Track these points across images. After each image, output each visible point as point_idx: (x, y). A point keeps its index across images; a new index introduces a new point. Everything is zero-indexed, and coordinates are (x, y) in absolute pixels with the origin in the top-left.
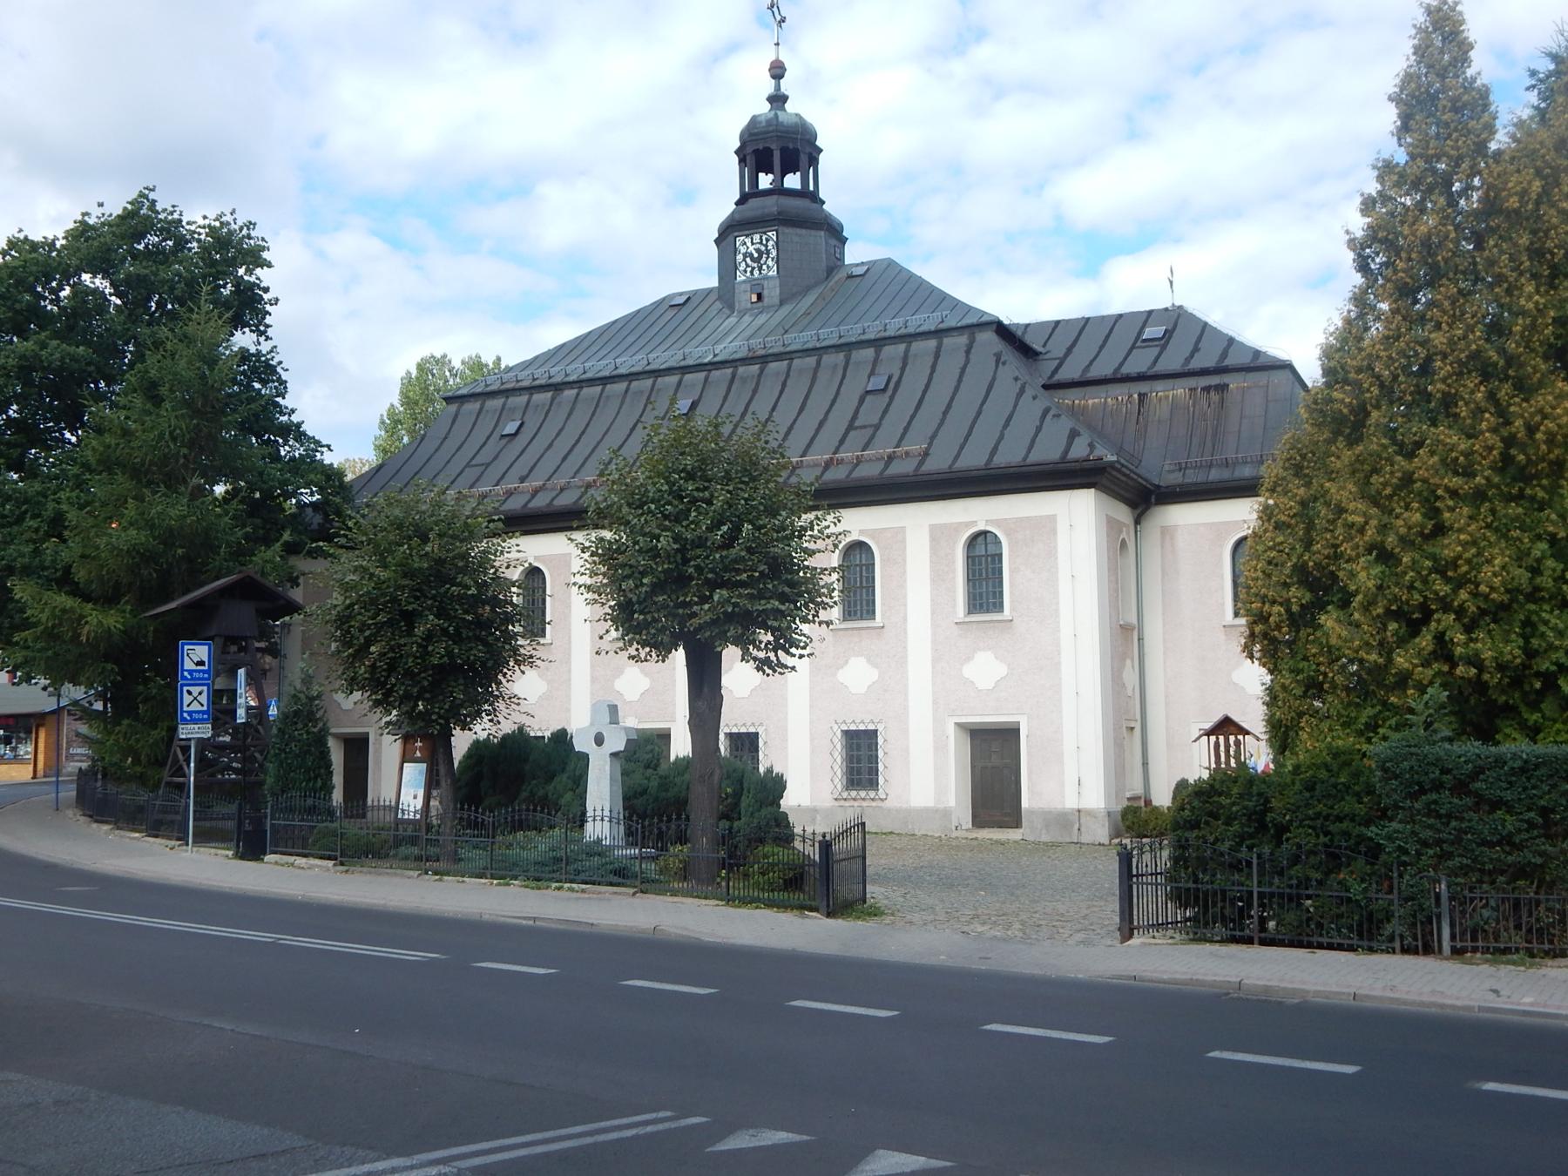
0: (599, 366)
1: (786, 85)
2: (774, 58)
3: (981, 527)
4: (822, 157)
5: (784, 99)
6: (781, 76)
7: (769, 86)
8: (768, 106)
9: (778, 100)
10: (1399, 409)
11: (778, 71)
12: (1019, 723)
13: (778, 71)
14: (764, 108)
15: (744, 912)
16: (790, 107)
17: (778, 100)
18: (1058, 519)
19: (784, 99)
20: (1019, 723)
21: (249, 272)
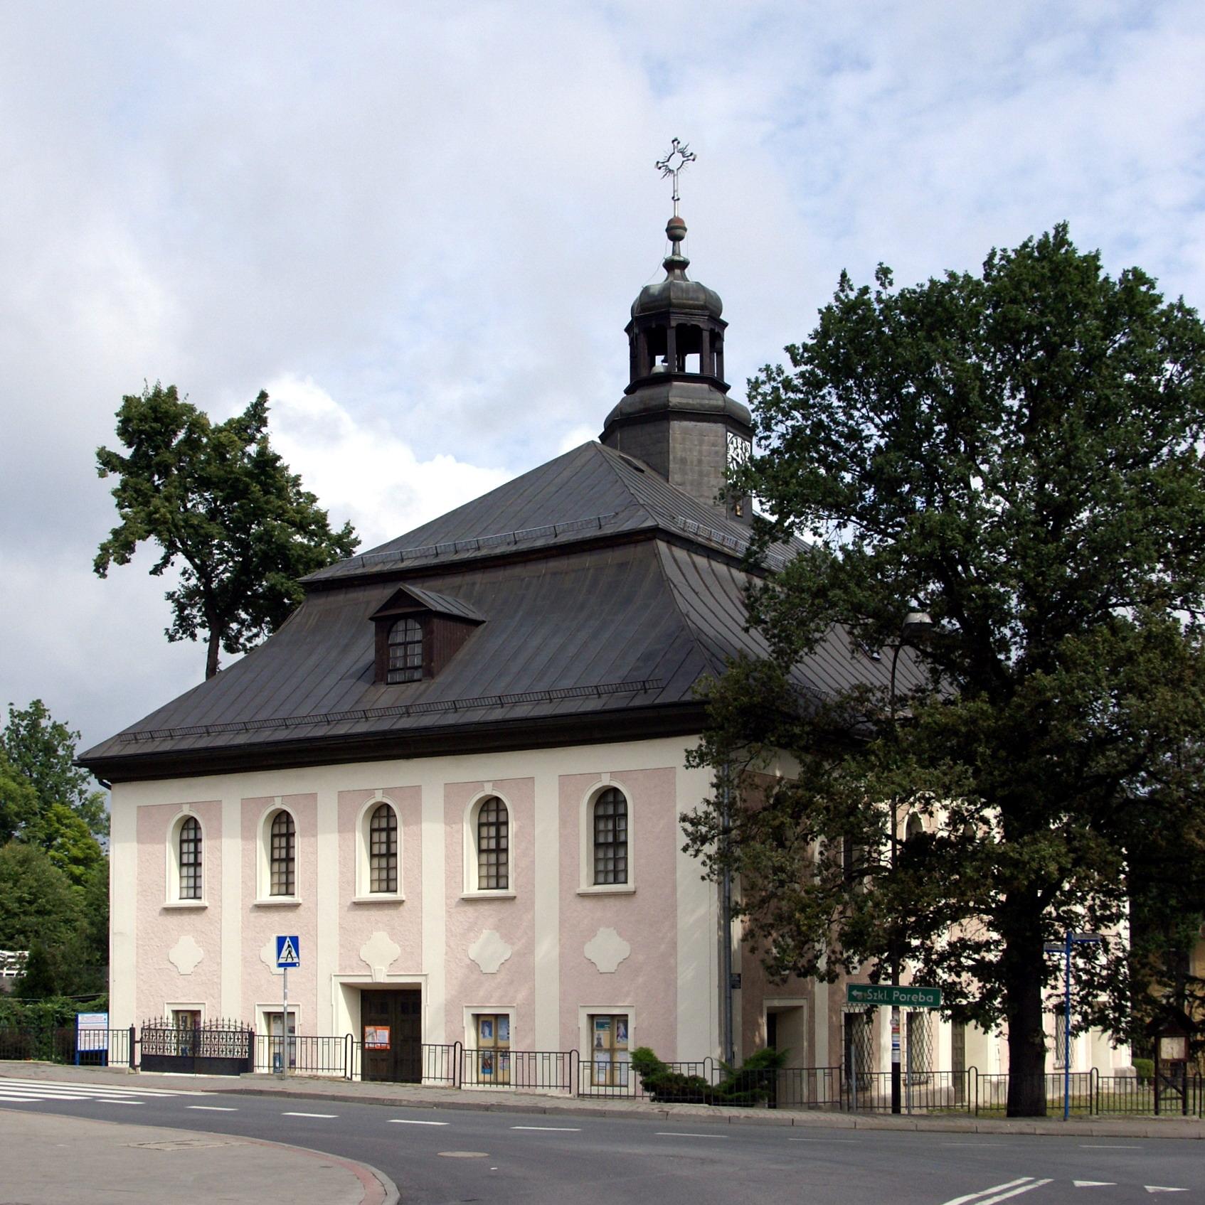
0: (495, 541)
1: (686, 249)
2: (672, 217)
3: (606, 781)
4: (727, 334)
5: (684, 265)
6: (680, 238)
7: (665, 249)
8: (664, 273)
9: (675, 265)
10: (1117, 730)
11: (675, 232)
12: (420, 984)
13: (675, 232)
14: (658, 277)
15: (477, 1102)
16: (692, 274)
17: (675, 265)
18: (319, 798)
19: (684, 265)
20: (420, 984)
21: (798, 349)
